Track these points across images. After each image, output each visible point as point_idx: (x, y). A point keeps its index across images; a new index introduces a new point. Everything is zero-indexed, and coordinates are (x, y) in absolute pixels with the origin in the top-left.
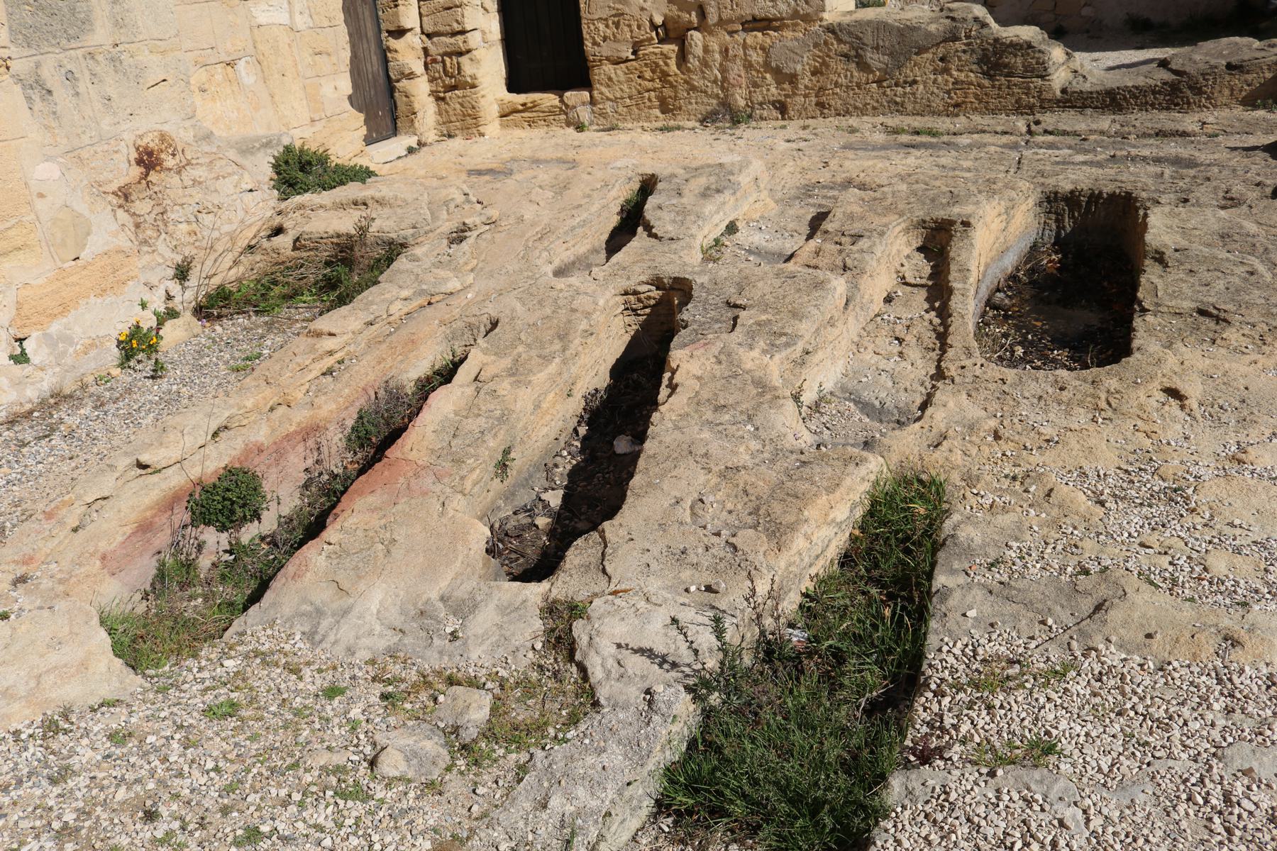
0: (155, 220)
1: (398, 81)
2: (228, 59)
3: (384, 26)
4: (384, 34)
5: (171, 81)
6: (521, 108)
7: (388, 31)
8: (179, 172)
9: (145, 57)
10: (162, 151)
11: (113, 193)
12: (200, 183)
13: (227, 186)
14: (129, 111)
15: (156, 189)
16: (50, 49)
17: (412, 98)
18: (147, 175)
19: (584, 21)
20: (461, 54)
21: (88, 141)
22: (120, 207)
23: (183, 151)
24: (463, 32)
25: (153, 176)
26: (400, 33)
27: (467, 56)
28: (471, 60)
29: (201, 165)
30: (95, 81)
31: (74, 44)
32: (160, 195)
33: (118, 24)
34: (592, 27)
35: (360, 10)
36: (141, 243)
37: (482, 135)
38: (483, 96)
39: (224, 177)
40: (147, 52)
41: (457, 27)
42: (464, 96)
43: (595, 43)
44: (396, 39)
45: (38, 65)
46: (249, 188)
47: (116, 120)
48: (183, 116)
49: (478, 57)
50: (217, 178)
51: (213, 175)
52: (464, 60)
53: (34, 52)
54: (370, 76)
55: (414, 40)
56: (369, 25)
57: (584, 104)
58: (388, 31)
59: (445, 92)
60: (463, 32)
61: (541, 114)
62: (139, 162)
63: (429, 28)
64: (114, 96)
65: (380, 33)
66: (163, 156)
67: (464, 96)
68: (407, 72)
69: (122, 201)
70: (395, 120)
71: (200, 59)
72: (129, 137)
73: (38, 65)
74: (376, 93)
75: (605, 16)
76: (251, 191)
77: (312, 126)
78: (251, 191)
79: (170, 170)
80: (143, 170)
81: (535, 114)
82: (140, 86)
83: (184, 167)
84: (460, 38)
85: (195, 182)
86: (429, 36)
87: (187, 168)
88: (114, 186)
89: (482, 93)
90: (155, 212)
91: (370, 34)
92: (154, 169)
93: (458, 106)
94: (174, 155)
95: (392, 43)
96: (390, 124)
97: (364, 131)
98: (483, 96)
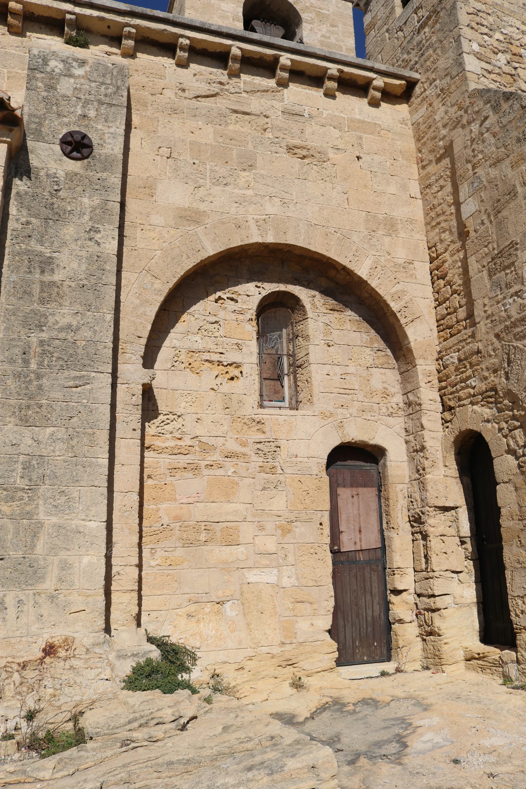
0: (34, 683)
1: (394, 624)
2: (218, 600)
3: (389, 586)
4: (389, 592)
5: (87, 611)
6: (477, 656)
7: (390, 590)
8: (65, 660)
9: (74, 597)
10: (60, 647)
11: (18, 664)
12: (75, 669)
13: (92, 674)
14: (53, 623)
15: (45, 666)
16: (14, 589)
17: (398, 637)
18: (44, 658)
19: (509, 597)
20: (434, 611)
21: (18, 635)
22: (17, 671)
23: (75, 649)
24: (433, 596)
25: (47, 660)
26: (397, 592)
27: (437, 613)
28: (440, 616)
29: (81, 659)
30: (37, 606)
31: (29, 587)
32: (45, 670)
33: (61, 580)
34: (514, 603)
35: (367, 575)
36: (16, 693)
37: (443, 672)
38: (446, 644)
39: (92, 668)
40: (76, 595)
41: (430, 592)
42: (435, 641)
43: (517, 615)
44: (396, 595)
45: (4, 596)
46: (106, 677)
47: (42, 627)
48: (91, 630)
49: (445, 614)
50: (87, 668)
51: (86, 666)
52: (435, 615)
53: (5, 589)
54: (369, 619)
55: (409, 598)
56: (375, 585)
57: (512, 662)
58: (390, 590)
59: (427, 636)
60: (433, 596)
61: (488, 664)
62: (44, 650)
63: (419, 592)
64: (45, 615)
65: (386, 591)
66: (60, 650)
67: (435, 641)
68: (397, 619)
69: (20, 669)
70: (390, 649)
71: (193, 599)
72: (46, 636)
73: (4, 596)
74: (374, 629)
75: (521, 595)
76: (107, 680)
77: (280, 647)
78: (107, 680)
79: (59, 658)
80: (43, 655)
81: (485, 663)
82: (65, 612)
83: (70, 658)
84: (432, 599)
85: (71, 667)
86: (419, 595)
87: (72, 659)
88: (21, 660)
89: (445, 641)
90: (36, 679)
91: (375, 590)
92: (49, 655)
93: (432, 647)
94: (67, 650)
95: (392, 598)
96: (385, 652)
97: (336, 655)
98: (446, 644)
